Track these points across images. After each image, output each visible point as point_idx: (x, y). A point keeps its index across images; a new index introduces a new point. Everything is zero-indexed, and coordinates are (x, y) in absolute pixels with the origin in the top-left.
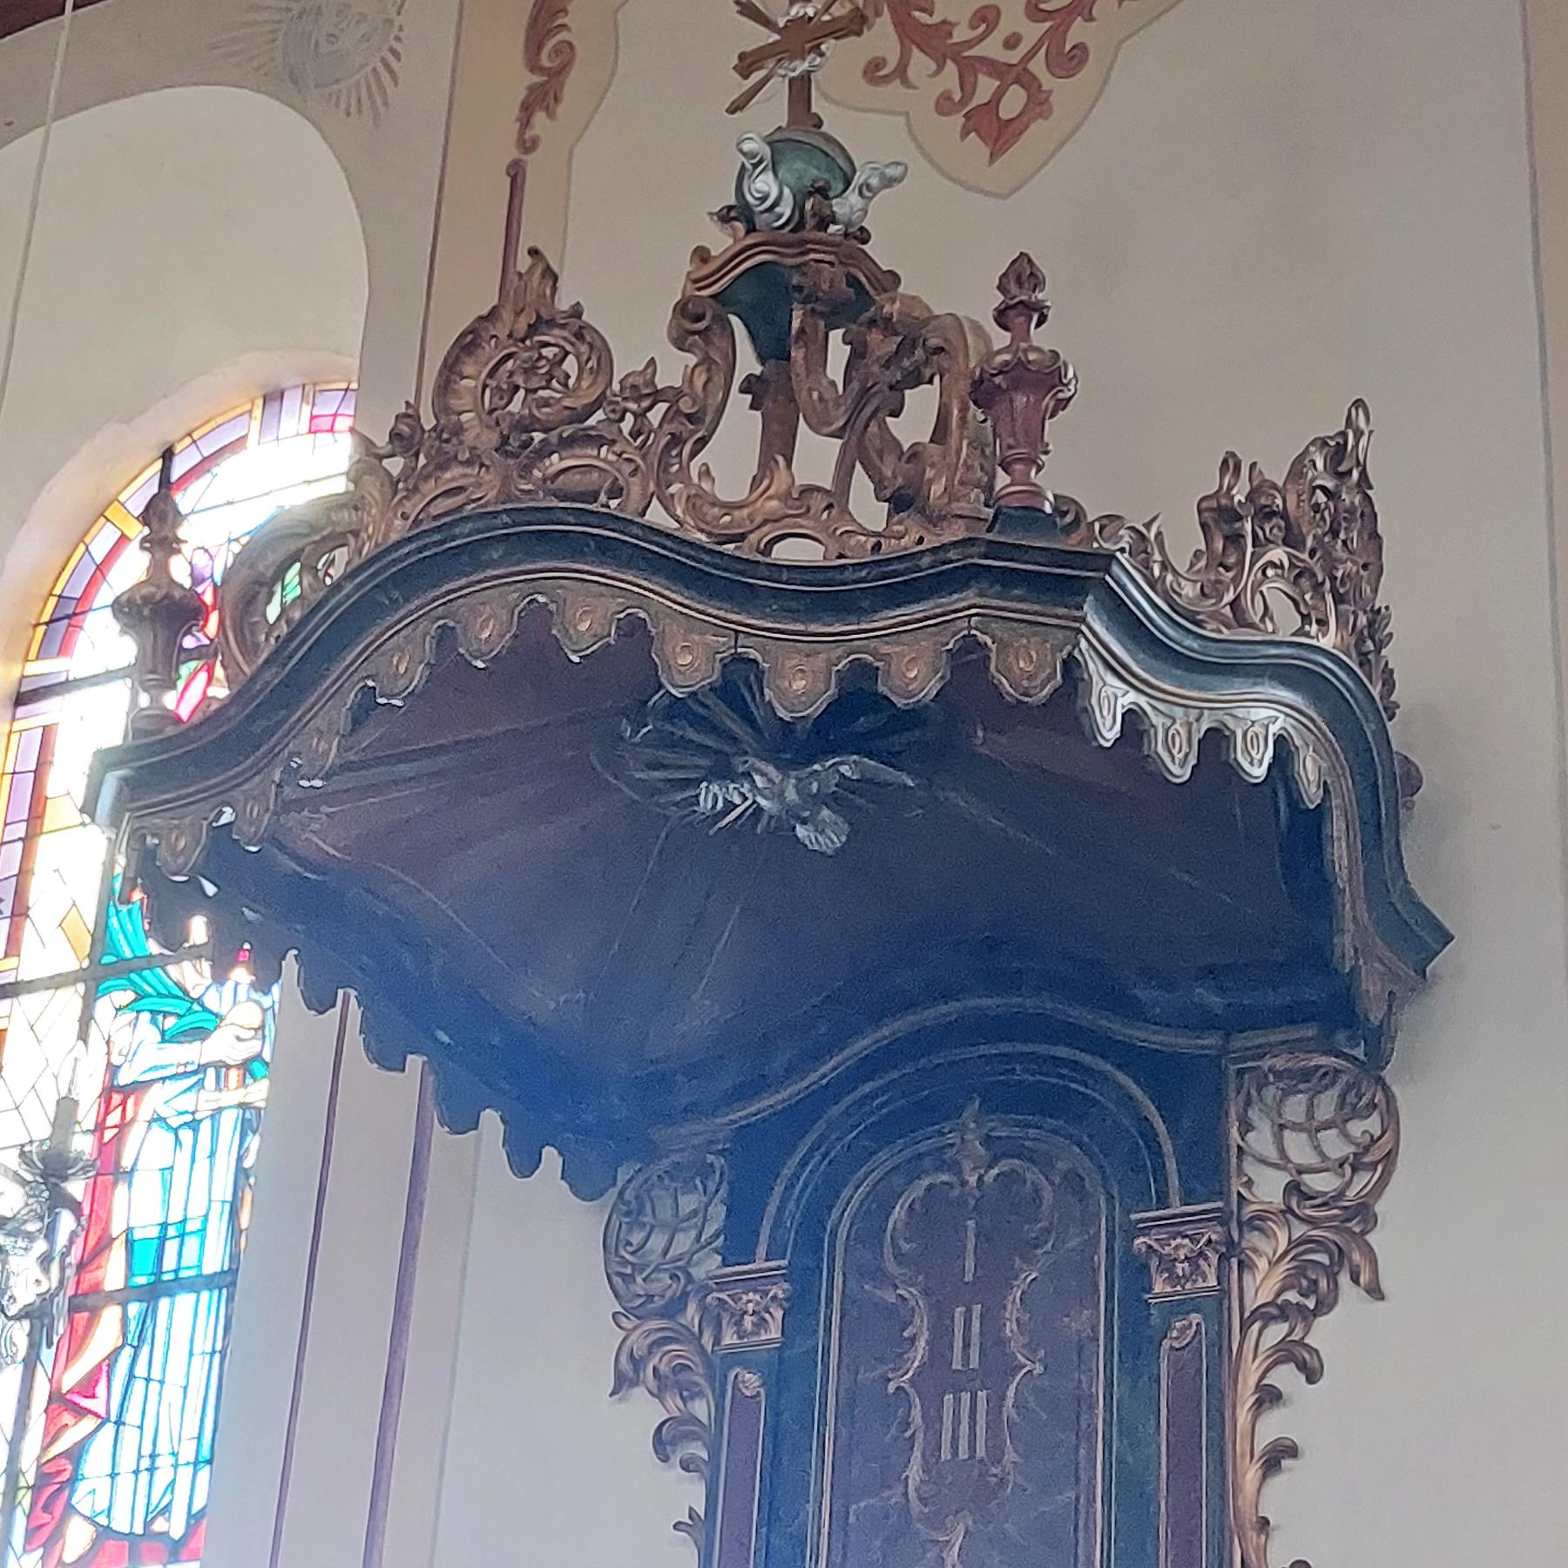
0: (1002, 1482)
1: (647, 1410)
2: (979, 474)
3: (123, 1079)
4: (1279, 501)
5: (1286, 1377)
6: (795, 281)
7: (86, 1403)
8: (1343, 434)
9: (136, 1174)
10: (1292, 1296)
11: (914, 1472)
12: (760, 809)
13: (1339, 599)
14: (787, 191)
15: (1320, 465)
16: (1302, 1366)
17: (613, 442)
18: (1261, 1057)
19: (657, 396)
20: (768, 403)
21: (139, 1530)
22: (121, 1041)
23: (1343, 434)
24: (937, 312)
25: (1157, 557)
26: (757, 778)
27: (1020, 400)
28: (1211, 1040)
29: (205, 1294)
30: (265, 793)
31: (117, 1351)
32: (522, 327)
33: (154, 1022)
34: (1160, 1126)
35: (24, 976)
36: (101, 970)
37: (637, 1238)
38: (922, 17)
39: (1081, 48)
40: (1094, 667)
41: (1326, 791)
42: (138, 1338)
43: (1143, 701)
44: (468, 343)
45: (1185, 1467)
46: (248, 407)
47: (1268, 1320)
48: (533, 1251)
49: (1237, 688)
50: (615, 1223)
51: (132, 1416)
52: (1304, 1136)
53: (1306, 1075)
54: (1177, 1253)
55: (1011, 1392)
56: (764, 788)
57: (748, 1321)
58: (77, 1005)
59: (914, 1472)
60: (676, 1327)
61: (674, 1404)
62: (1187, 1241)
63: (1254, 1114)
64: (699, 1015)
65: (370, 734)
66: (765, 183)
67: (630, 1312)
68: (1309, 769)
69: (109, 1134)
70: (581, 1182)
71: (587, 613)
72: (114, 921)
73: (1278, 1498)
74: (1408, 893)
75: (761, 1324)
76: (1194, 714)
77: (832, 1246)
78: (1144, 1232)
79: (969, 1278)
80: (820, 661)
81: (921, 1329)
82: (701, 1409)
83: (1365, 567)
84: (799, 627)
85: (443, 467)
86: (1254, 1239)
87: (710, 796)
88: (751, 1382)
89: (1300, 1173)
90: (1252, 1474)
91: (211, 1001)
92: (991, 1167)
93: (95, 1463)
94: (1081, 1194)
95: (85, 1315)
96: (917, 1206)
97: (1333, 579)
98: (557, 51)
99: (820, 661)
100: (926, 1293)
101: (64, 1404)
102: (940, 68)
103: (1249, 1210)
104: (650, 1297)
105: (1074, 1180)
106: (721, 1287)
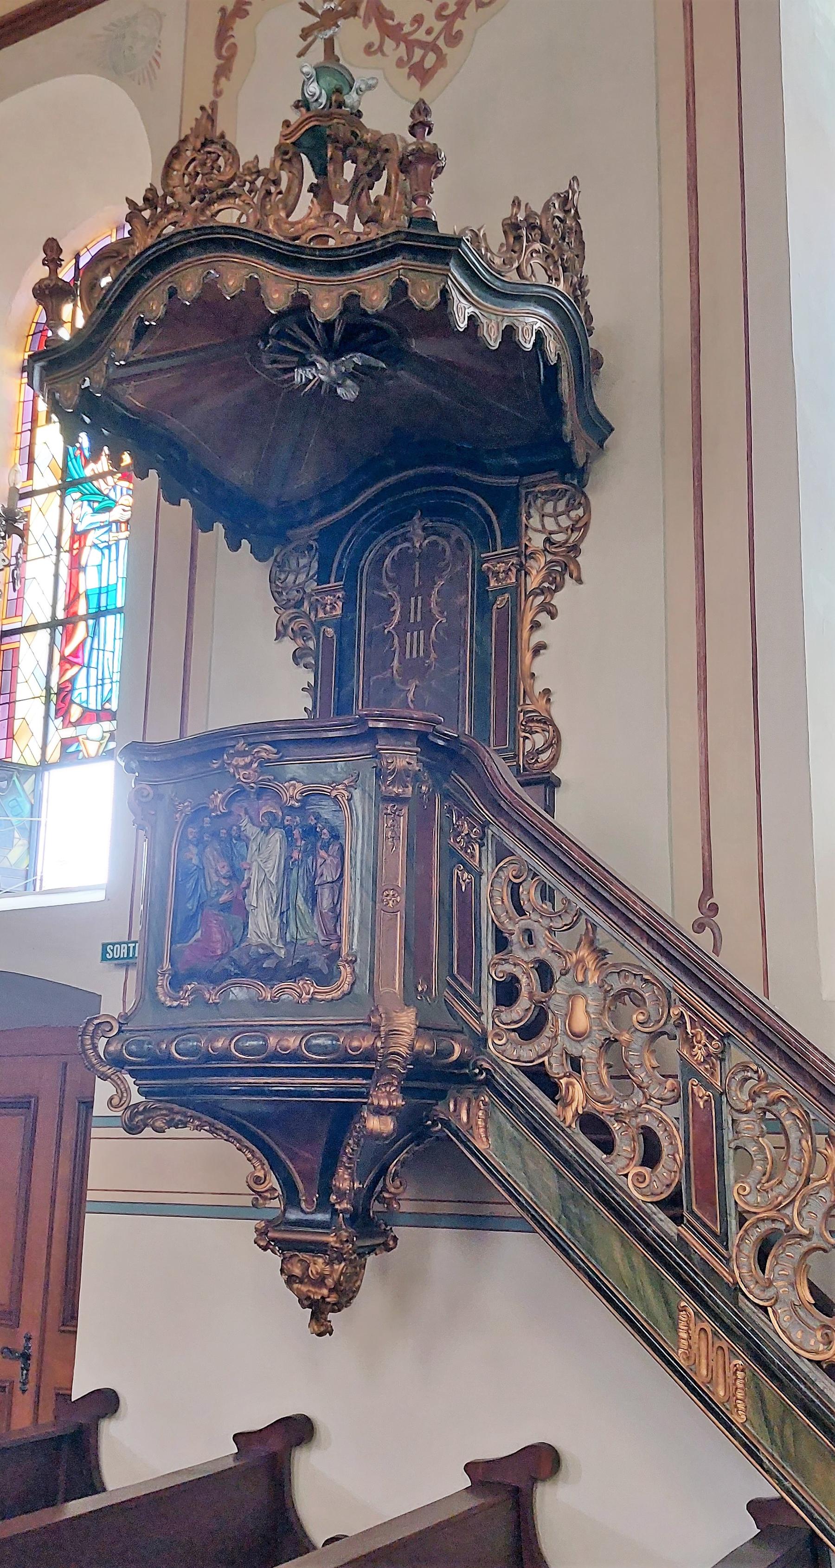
0: (430, 666)
1: (289, 646)
2: (405, 207)
3: (80, 528)
4: (538, 221)
5: (543, 618)
6: (328, 133)
7: (75, 660)
8: (567, 192)
9: (88, 568)
10: (546, 585)
11: (396, 663)
12: (322, 382)
13: (565, 270)
14: (323, 92)
15: (557, 206)
16: (549, 613)
17: (240, 195)
18: (535, 486)
19: (258, 173)
20: (320, 196)
21: (99, 708)
22: (77, 514)
23: (567, 192)
24: (383, 133)
25: (483, 244)
26: (318, 365)
27: (421, 167)
28: (515, 480)
29: (118, 615)
30: (101, 370)
31: (85, 639)
32: (199, 146)
33: (89, 505)
34: (494, 518)
35: (37, 487)
36: (67, 484)
37: (283, 577)
38: (390, 22)
39: (459, 32)
40: (455, 294)
41: (559, 358)
42: (94, 633)
43: (477, 311)
44: (175, 154)
45: (501, 653)
46: (109, 233)
47: (537, 595)
48: (241, 580)
49: (521, 307)
50: (274, 571)
51: (93, 664)
52: (552, 519)
53: (554, 492)
54: (500, 570)
56: (321, 371)
57: (328, 607)
58: (58, 499)
59: (396, 663)
61: (300, 642)
63: (532, 511)
64: (304, 480)
65: (147, 344)
66: (313, 88)
67: (282, 607)
68: (552, 347)
69: (75, 552)
70: (259, 554)
71: (233, 275)
72: (70, 463)
73: (539, 666)
74: (596, 409)
76: (500, 318)
77: (362, 575)
78: (486, 562)
79: (416, 585)
80: (335, 294)
81: (397, 607)
82: (311, 644)
83: (577, 256)
84: (325, 278)
85: (168, 212)
86: (531, 562)
87: (300, 375)
88: (330, 631)
89: (550, 534)
90: (528, 656)
91: (112, 495)
93: (81, 682)
95: (72, 625)
96: (396, 558)
97: (562, 260)
98: (229, 48)
99: (335, 294)
100: (399, 593)
101: (66, 661)
102: (398, 45)
103: (529, 552)
104: (289, 600)
106: (317, 594)
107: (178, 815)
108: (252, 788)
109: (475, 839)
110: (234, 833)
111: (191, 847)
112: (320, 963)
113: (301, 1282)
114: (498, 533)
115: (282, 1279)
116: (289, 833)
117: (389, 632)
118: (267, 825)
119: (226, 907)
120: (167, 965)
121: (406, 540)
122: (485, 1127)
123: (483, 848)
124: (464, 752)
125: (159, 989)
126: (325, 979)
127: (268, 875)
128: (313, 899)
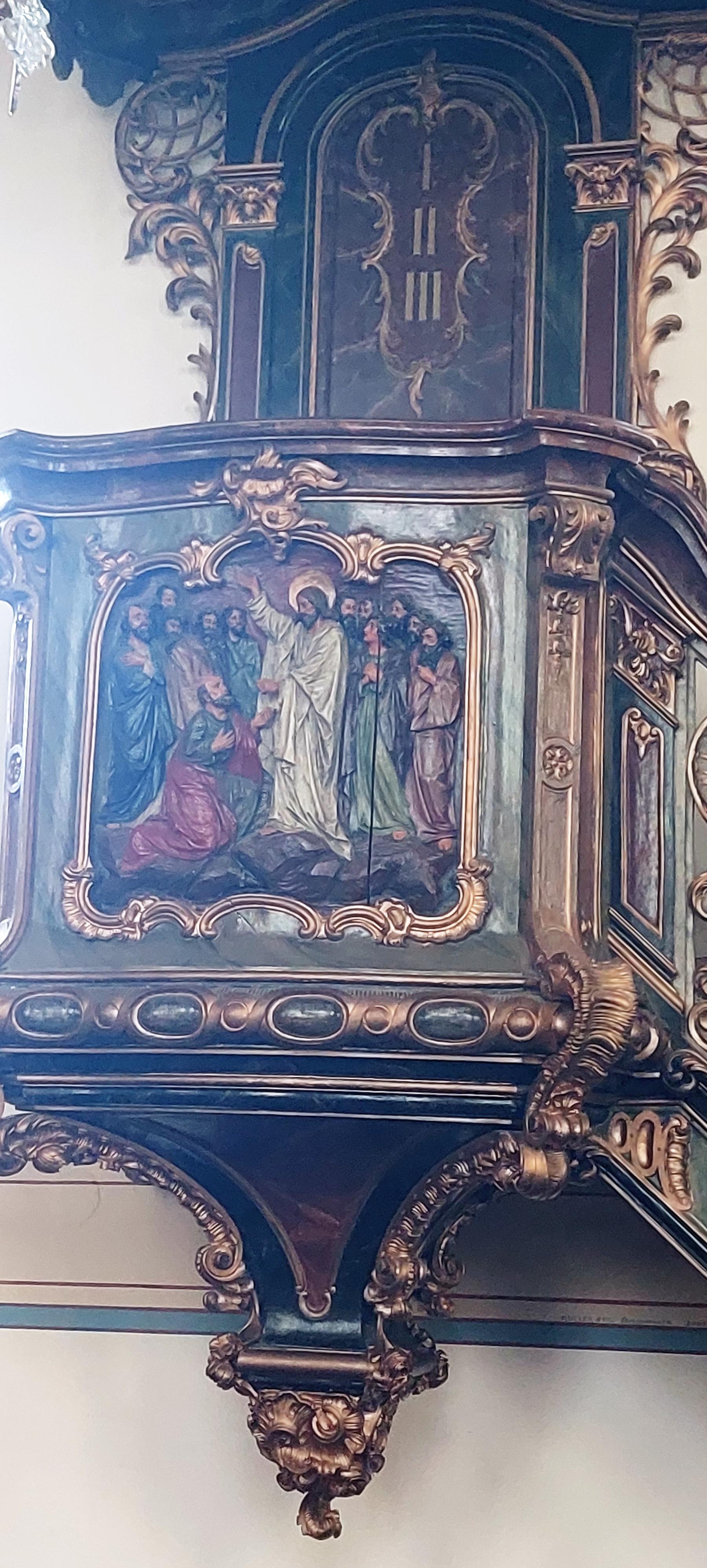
5: (674, 272)
11: (384, 327)
55: (461, 272)
59: (384, 327)
60: (181, 209)
61: (180, 269)
62: (606, 168)
63: (651, 79)
75: (259, 210)
78: (572, 159)
79: (426, 187)
81: (387, 222)
82: (203, 273)
88: (252, 254)
90: (648, 340)
92: (443, 104)
94: (516, 129)
96: (382, 130)
100: (391, 196)
105: (510, 121)
107: (102, 580)
108: (281, 540)
109: (669, 665)
110: (233, 623)
111: (135, 642)
112: (420, 870)
113: (295, 1443)
114: (595, 112)
115: (251, 1439)
116: (353, 633)
117: (370, 266)
118: (312, 612)
119: (222, 760)
120: (84, 862)
121: (406, 101)
122: (684, 1174)
123: (682, 682)
124: (655, 505)
125: (68, 907)
126: (426, 902)
127: (317, 707)
128: (404, 756)
